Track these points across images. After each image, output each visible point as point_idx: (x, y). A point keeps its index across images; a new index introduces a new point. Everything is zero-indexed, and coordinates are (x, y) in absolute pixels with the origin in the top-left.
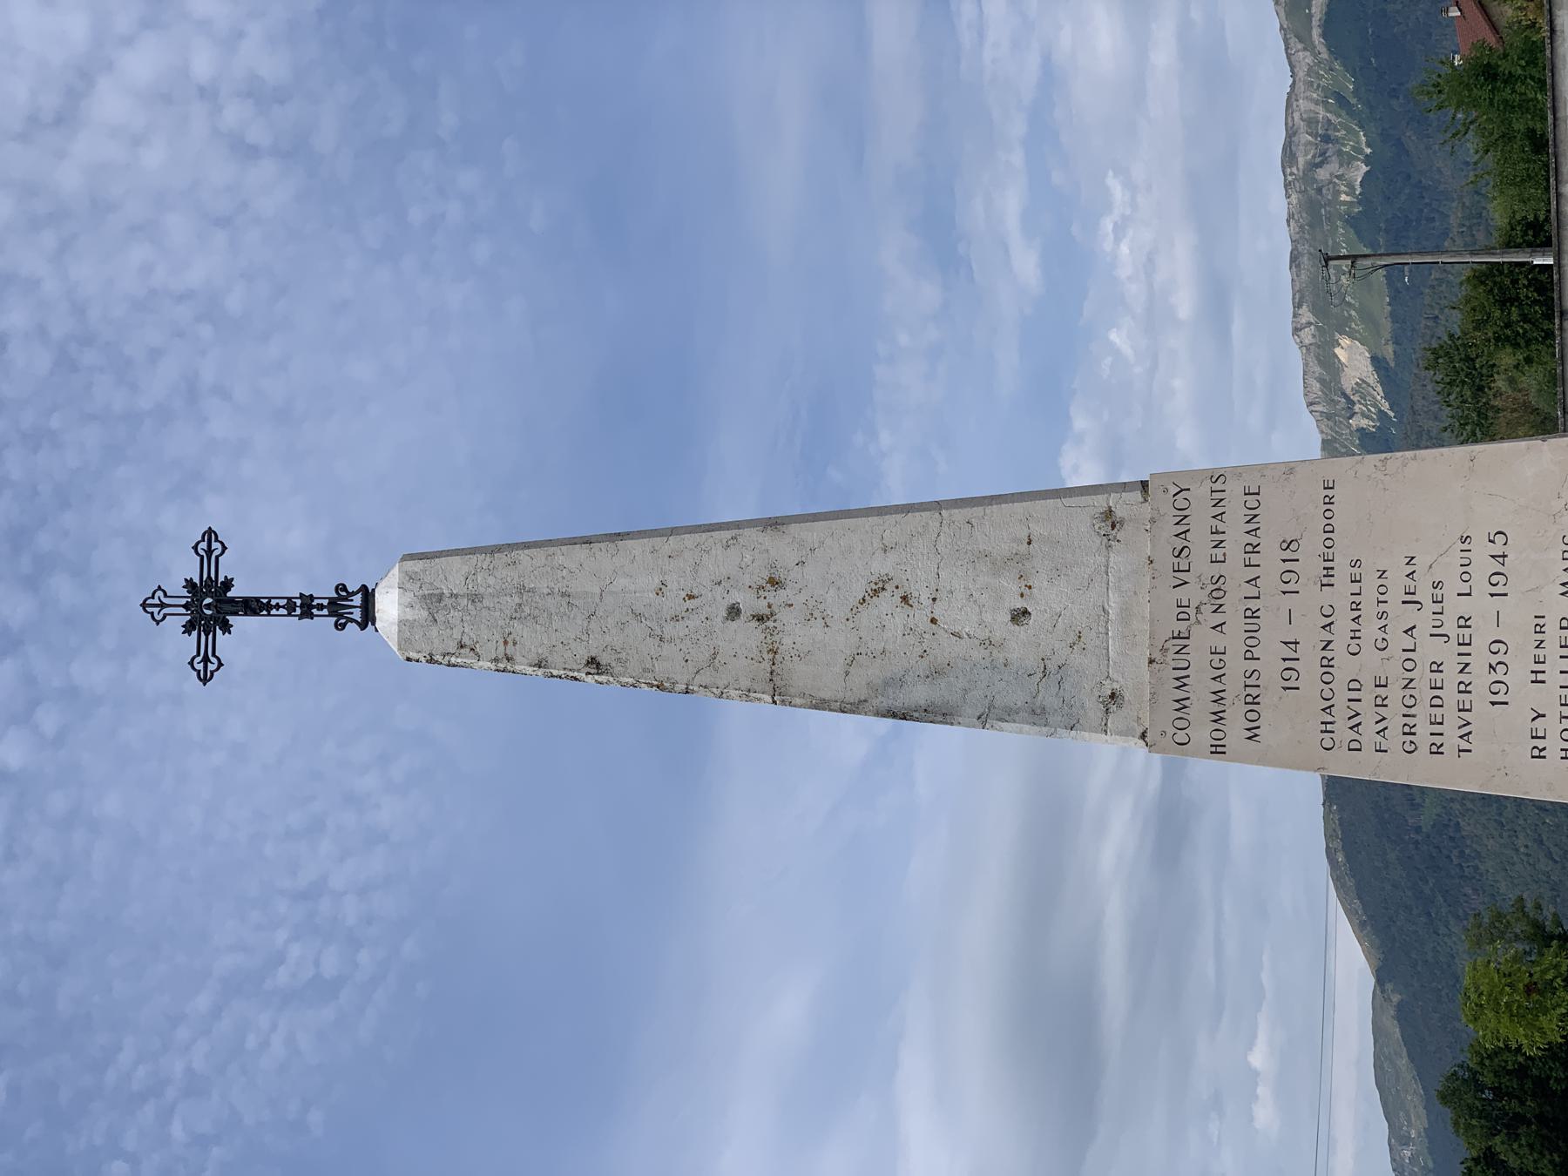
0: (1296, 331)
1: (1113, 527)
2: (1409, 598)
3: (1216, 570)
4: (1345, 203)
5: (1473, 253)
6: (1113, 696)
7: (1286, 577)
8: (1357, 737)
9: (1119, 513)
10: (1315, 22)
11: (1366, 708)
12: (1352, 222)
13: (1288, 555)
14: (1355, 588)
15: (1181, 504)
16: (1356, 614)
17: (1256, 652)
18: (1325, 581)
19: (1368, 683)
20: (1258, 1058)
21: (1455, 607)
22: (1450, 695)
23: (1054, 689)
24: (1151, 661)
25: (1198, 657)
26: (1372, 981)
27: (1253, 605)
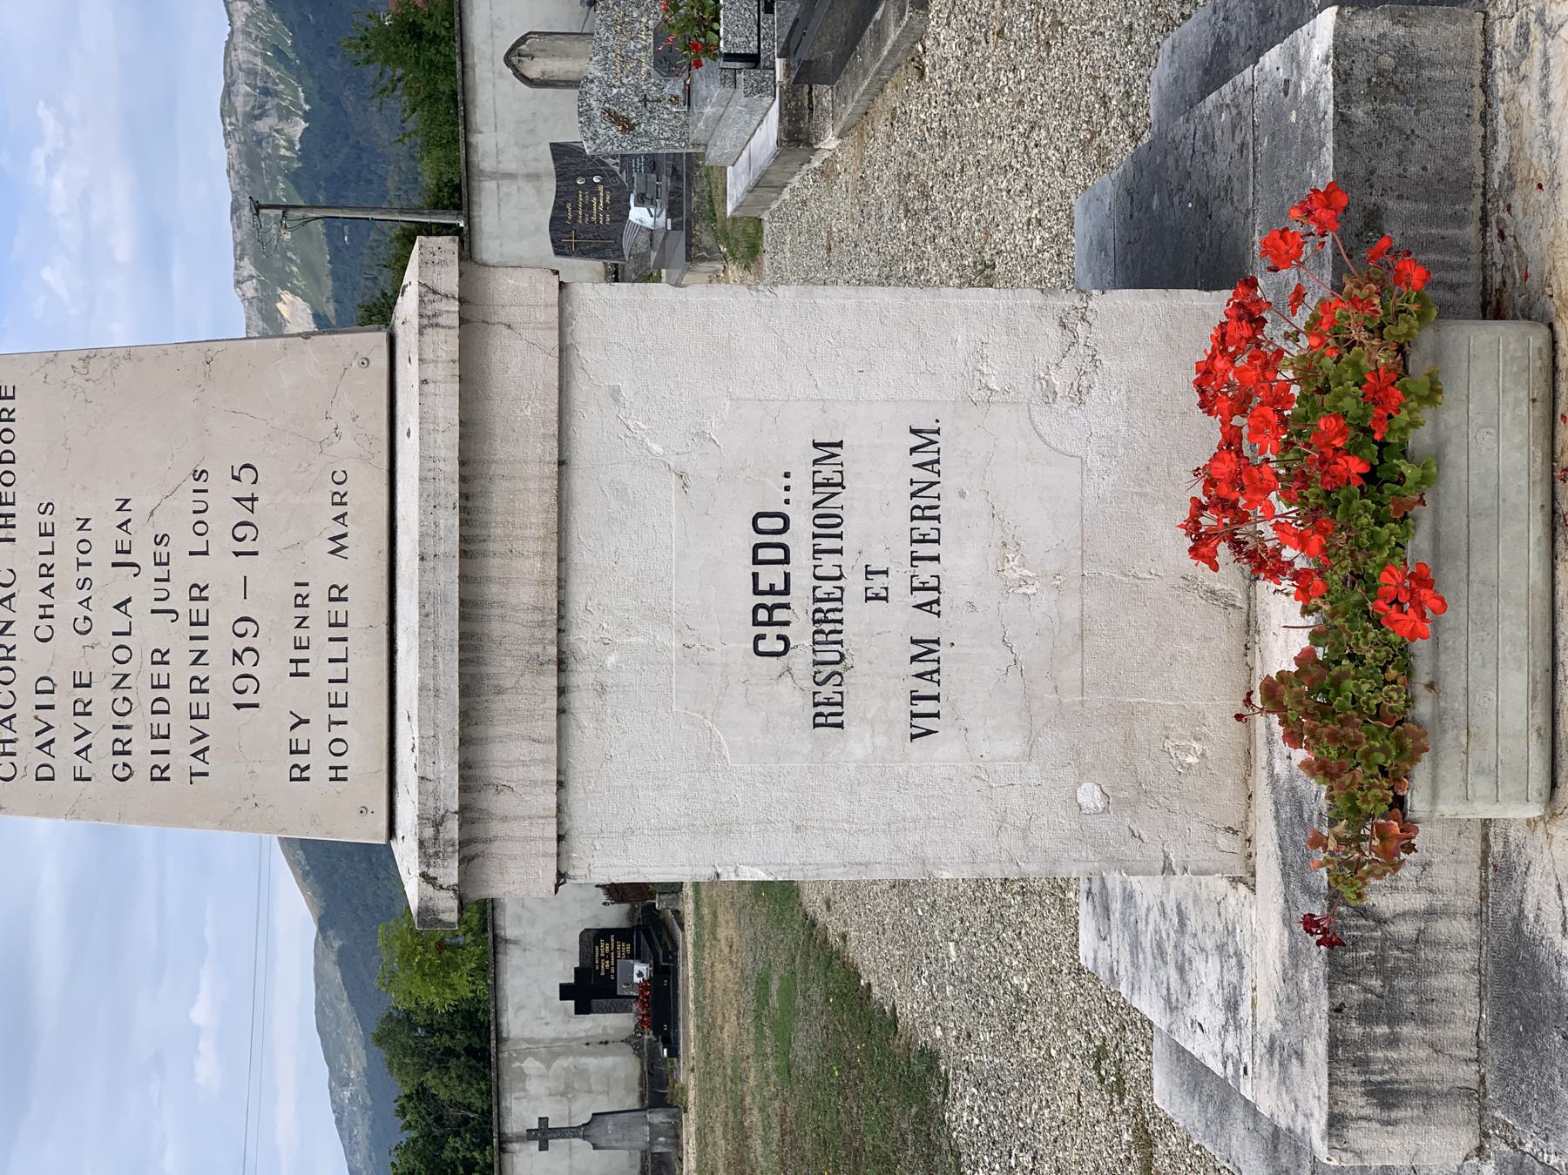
0: (238, 283)
4: (284, 158)
5: (402, 211)
8: (48, 760)
12: (294, 178)
14: (45, 544)
20: (201, 1014)
21: (185, 571)
22: (179, 697)
26: (315, 928)
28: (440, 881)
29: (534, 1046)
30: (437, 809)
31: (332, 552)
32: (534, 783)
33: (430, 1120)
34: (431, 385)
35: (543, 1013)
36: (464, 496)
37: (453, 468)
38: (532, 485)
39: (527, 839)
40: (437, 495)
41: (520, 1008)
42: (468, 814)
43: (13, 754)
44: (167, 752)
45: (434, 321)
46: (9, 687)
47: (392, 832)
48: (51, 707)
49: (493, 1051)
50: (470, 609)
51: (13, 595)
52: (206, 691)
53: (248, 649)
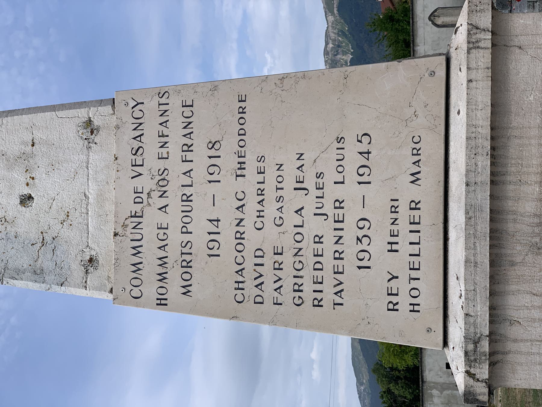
1: (92, 133)
2: (299, 185)
3: (162, 164)
6: (91, 260)
7: (211, 170)
9: (96, 122)
10: (335, 6)
11: (267, 270)
13: (213, 153)
14: (260, 178)
15: (138, 114)
16: (261, 198)
17: (190, 228)
18: (239, 172)
19: (269, 251)
21: (332, 192)
22: (328, 261)
23: (49, 255)
24: (116, 235)
25: (148, 230)
27: (188, 191)
28: (478, 376)
29: (436, 386)
30: (476, 333)
31: (412, 182)
32: (534, 320)
33: (392, 401)
34: (474, 83)
35: (439, 373)
36: (493, 148)
37: (486, 131)
38: (533, 142)
39: (529, 354)
40: (477, 147)
41: (430, 370)
42: (494, 337)
43: (243, 289)
44: (321, 291)
45: (477, 45)
46: (242, 254)
47: (445, 343)
48: (262, 265)
49: (421, 385)
50: (496, 215)
51: (244, 205)
52: (342, 259)
53: (365, 236)
